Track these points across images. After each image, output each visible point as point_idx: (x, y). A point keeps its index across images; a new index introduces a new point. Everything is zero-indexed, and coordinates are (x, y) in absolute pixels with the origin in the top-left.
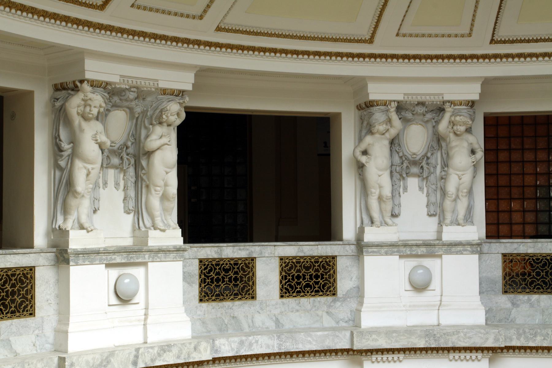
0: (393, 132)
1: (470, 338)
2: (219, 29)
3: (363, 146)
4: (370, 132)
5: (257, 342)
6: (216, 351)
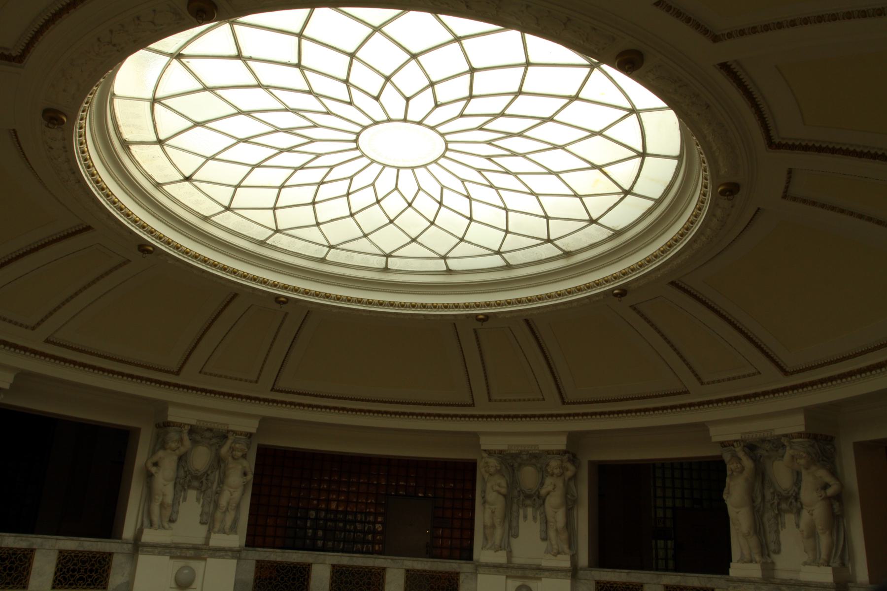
0: (183, 450)
2: (47, 341)
3: (155, 459)
4: (163, 447)
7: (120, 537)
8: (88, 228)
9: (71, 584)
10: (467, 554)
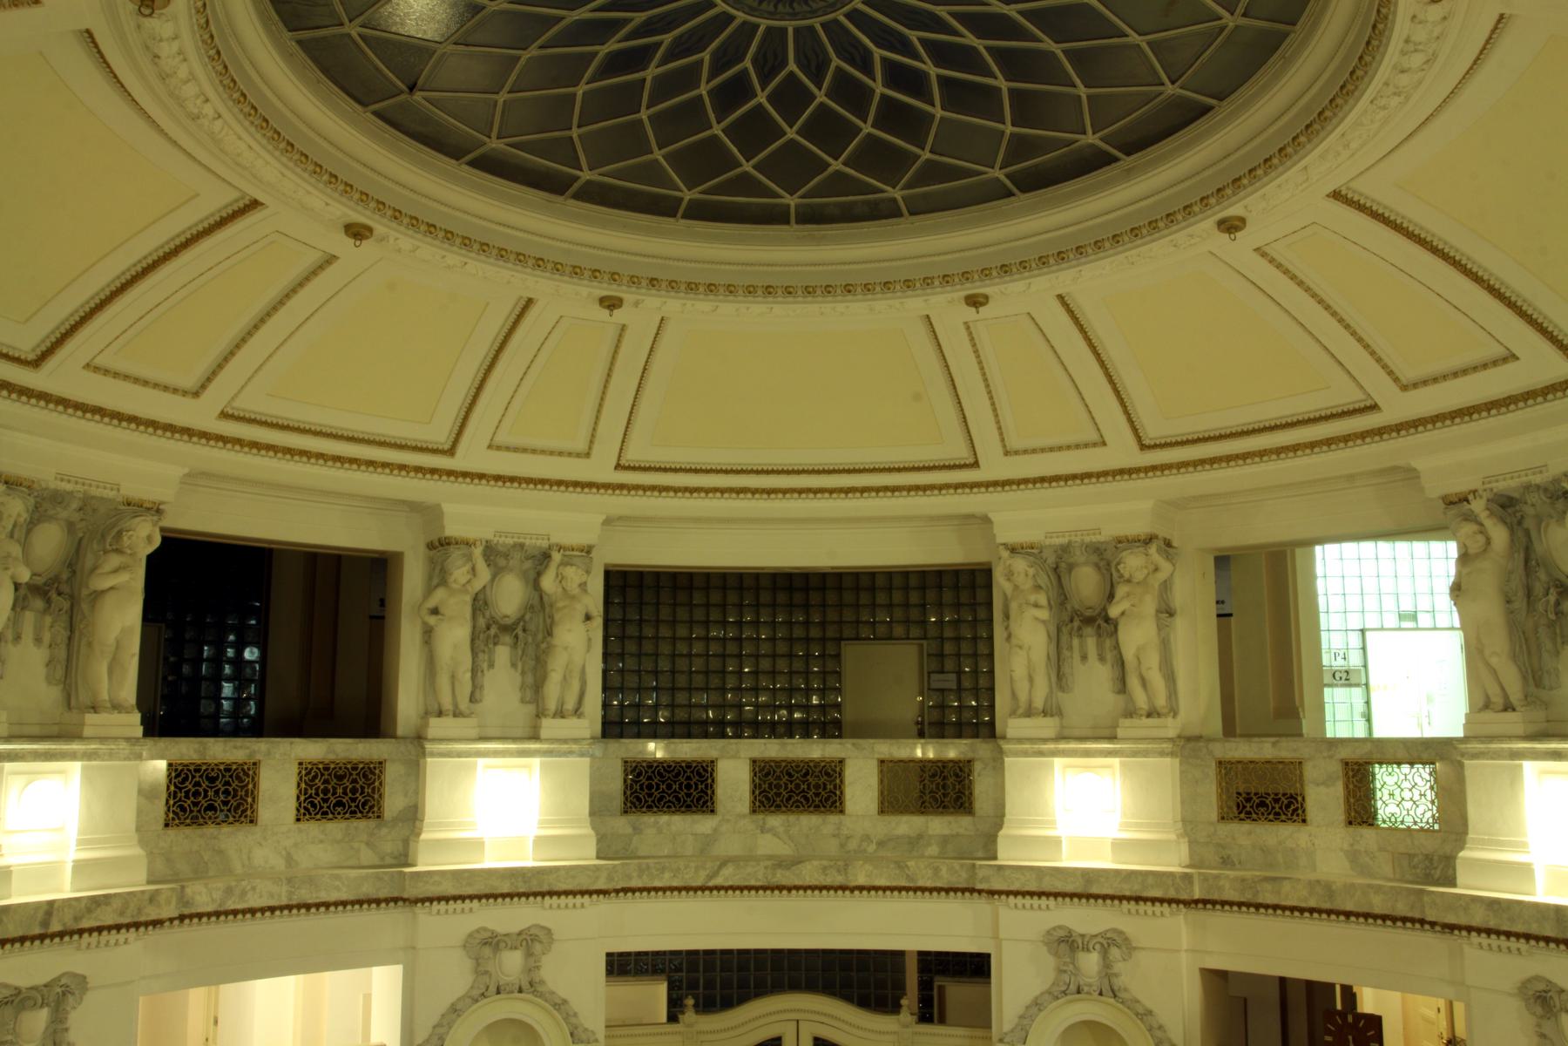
0: (478, 585)
1: (573, 877)
2: (224, 415)
3: (431, 603)
4: (443, 582)
5: (254, 889)
6: (187, 904)
9: (325, 813)
10: (985, 728)
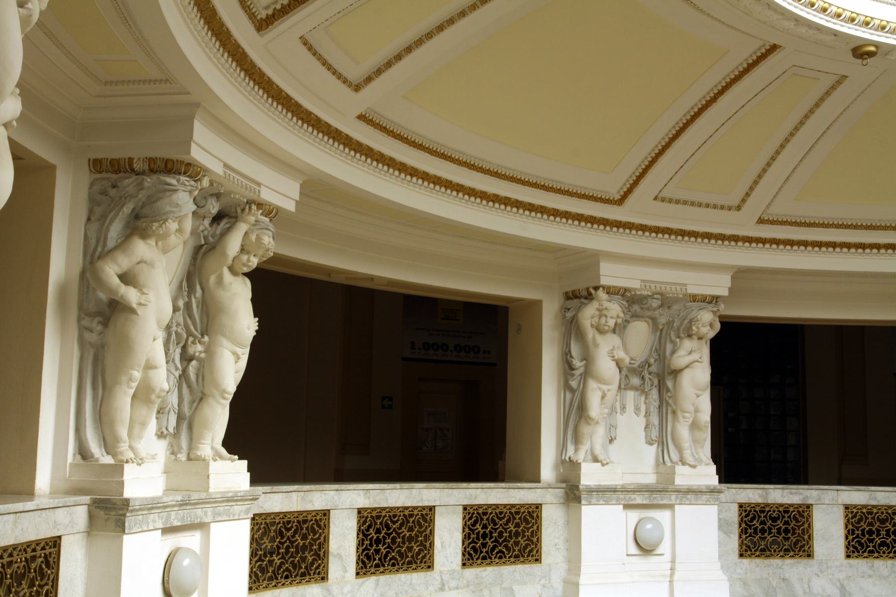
2: (761, 221)
7: (538, 480)
8: (774, 48)
